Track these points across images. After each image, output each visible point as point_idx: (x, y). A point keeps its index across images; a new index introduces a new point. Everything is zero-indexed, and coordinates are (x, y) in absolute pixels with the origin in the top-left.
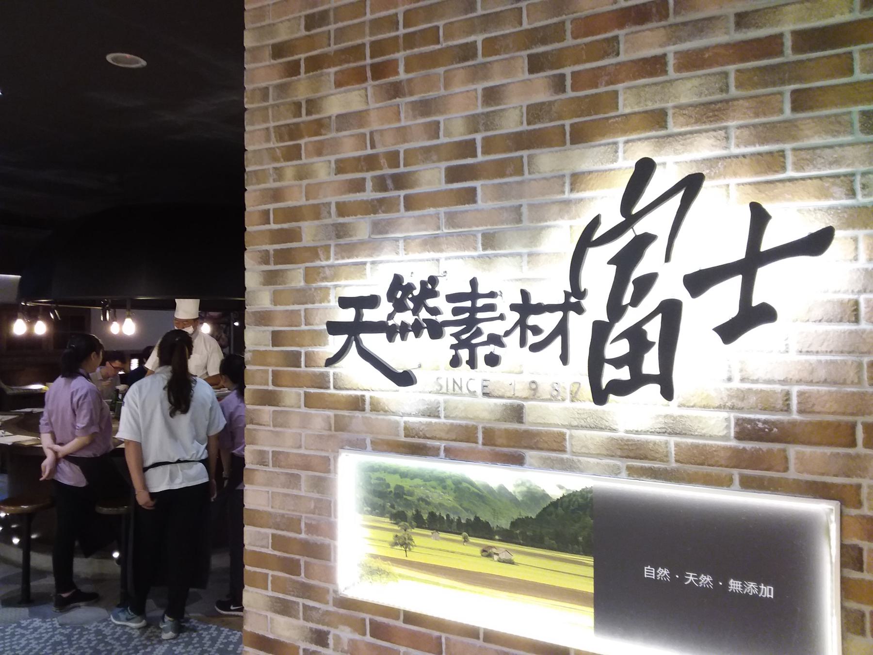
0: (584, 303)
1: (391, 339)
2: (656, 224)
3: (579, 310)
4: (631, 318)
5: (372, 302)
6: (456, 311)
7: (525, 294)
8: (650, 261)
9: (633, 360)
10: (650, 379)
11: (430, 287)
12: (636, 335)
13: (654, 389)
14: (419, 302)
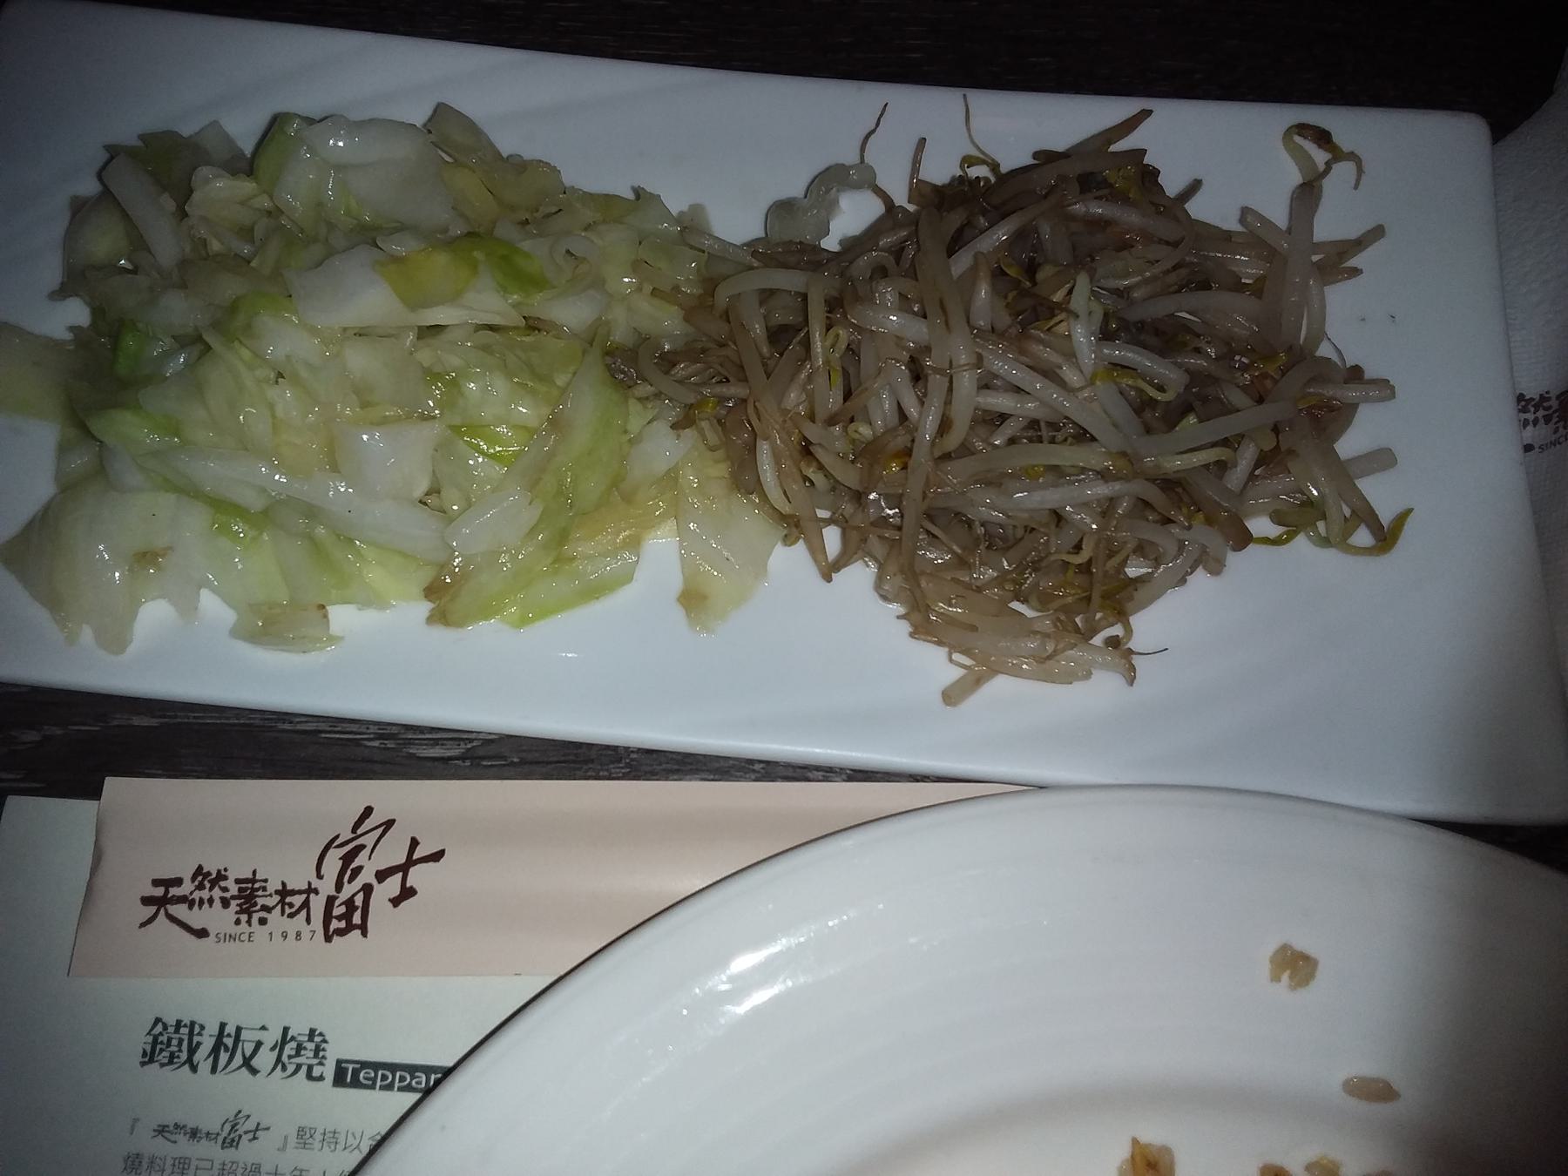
0: (186, 1021)
1: (191, 908)
2: (369, 840)
3: (316, 892)
5: (178, 882)
6: (240, 890)
7: (284, 884)
9: (347, 916)
11: (221, 876)
12: (350, 903)
13: (358, 932)
14: (214, 883)
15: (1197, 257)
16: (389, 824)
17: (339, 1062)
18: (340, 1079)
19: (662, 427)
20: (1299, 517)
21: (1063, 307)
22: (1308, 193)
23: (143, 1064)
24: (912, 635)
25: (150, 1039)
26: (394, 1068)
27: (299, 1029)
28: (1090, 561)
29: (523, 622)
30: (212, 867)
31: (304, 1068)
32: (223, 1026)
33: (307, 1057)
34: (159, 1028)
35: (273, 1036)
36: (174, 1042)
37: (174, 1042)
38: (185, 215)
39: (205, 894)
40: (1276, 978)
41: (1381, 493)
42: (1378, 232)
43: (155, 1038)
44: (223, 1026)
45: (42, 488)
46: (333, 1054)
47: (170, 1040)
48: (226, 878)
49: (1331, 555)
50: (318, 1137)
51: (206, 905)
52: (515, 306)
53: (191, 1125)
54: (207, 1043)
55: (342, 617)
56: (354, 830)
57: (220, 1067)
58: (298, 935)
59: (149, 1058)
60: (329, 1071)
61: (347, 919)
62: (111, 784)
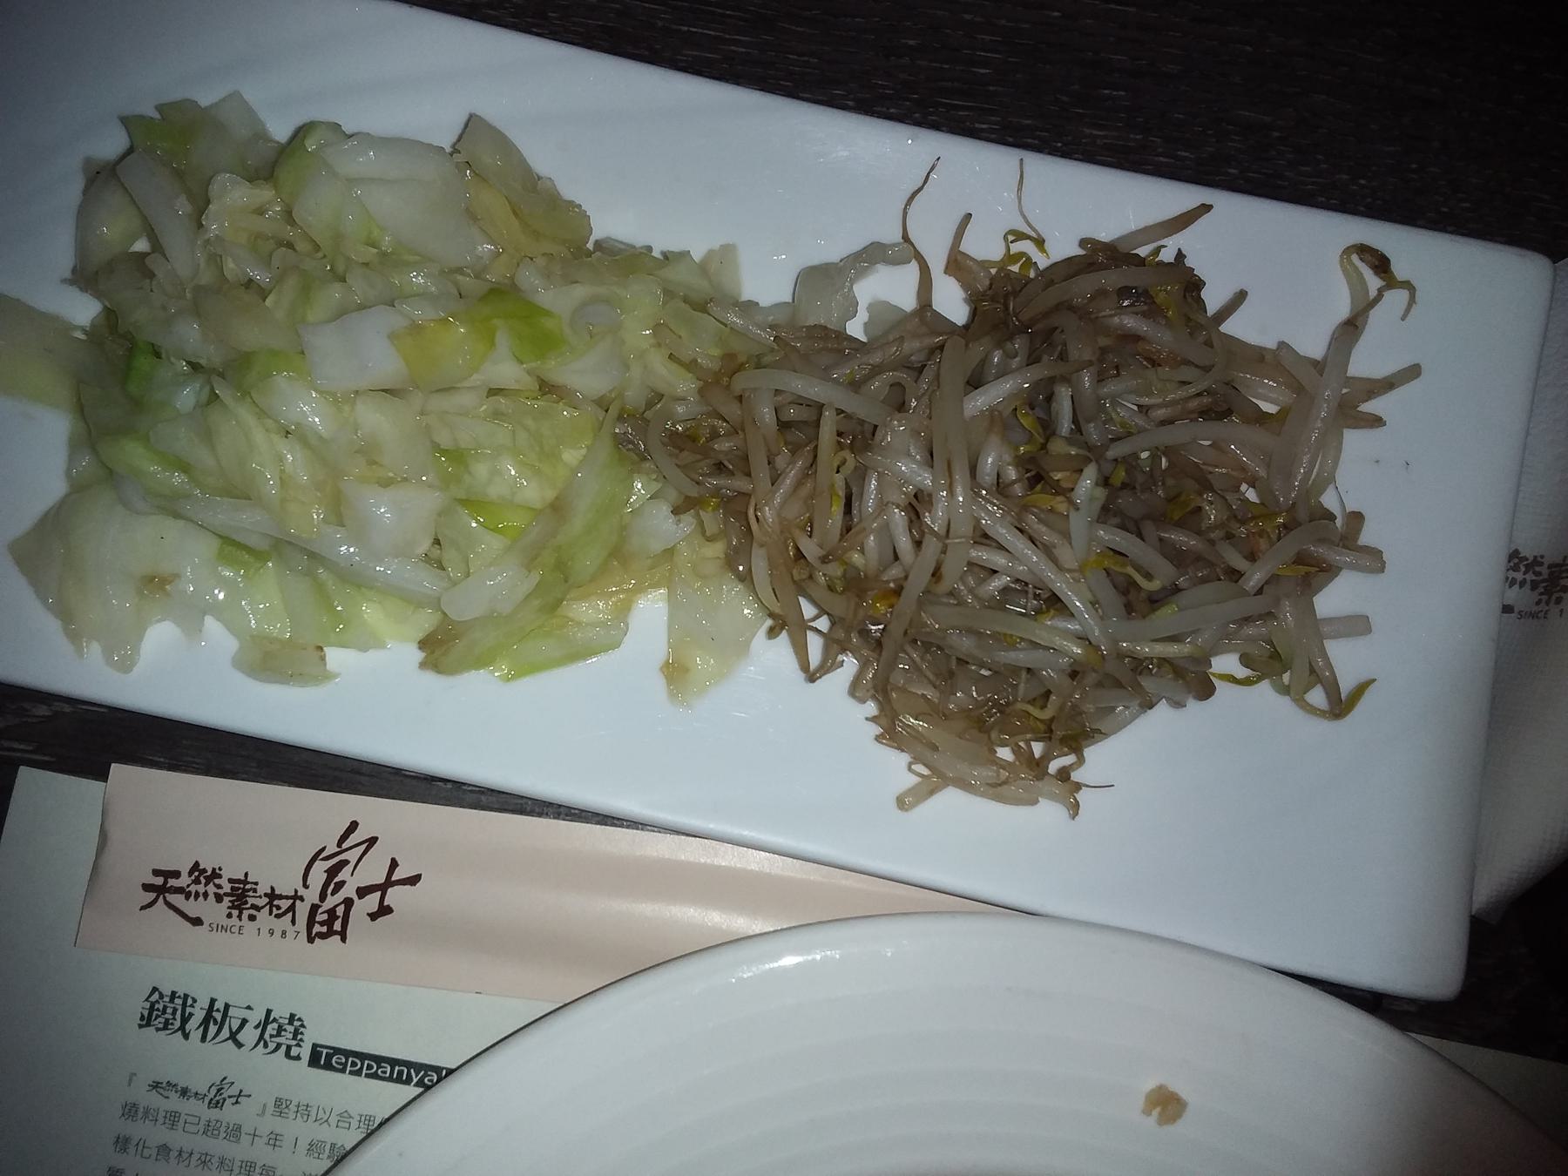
1: (187, 898)
2: (352, 856)
3: (302, 899)
4: (331, 901)
5: (177, 874)
8: (343, 875)
9: (329, 924)
10: (336, 933)
11: (216, 874)
12: (332, 912)
14: (209, 880)
15: (1221, 379)
16: (372, 841)
17: (315, 1046)
18: (314, 1061)
19: (664, 509)
20: (1268, 664)
21: (1066, 492)
22: (1352, 328)
23: (141, 1026)
24: (878, 738)
25: (148, 1005)
26: (362, 1056)
27: (280, 1013)
28: (1052, 720)
29: (507, 679)
30: (207, 865)
31: (284, 1048)
32: (213, 1001)
33: (287, 1038)
34: (156, 996)
35: (257, 1016)
36: (169, 1011)
37: (169, 1011)
38: (201, 226)
39: (201, 888)
40: (1147, 1112)
41: (1347, 660)
42: (1412, 372)
43: (152, 1005)
44: (213, 1001)
45: (55, 488)
46: (310, 1037)
47: (165, 1008)
48: (220, 876)
49: (1284, 704)
50: (293, 1108)
51: (201, 898)
52: (529, 373)
53: (182, 1084)
54: (199, 1015)
55: (335, 657)
56: (339, 845)
57: (210, 1037)
58: (284, 933)
59: (146, 1021)
60: (306, 1052)
61: (329, 924)
62: (116, 769)
